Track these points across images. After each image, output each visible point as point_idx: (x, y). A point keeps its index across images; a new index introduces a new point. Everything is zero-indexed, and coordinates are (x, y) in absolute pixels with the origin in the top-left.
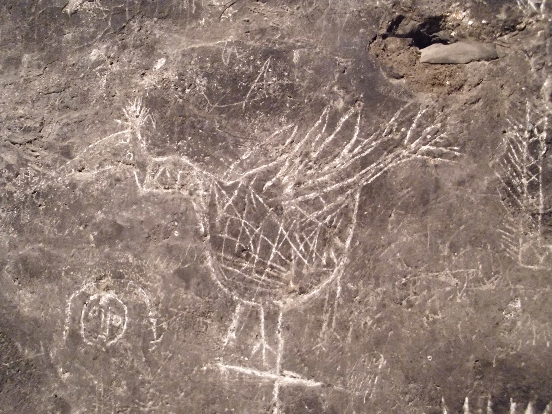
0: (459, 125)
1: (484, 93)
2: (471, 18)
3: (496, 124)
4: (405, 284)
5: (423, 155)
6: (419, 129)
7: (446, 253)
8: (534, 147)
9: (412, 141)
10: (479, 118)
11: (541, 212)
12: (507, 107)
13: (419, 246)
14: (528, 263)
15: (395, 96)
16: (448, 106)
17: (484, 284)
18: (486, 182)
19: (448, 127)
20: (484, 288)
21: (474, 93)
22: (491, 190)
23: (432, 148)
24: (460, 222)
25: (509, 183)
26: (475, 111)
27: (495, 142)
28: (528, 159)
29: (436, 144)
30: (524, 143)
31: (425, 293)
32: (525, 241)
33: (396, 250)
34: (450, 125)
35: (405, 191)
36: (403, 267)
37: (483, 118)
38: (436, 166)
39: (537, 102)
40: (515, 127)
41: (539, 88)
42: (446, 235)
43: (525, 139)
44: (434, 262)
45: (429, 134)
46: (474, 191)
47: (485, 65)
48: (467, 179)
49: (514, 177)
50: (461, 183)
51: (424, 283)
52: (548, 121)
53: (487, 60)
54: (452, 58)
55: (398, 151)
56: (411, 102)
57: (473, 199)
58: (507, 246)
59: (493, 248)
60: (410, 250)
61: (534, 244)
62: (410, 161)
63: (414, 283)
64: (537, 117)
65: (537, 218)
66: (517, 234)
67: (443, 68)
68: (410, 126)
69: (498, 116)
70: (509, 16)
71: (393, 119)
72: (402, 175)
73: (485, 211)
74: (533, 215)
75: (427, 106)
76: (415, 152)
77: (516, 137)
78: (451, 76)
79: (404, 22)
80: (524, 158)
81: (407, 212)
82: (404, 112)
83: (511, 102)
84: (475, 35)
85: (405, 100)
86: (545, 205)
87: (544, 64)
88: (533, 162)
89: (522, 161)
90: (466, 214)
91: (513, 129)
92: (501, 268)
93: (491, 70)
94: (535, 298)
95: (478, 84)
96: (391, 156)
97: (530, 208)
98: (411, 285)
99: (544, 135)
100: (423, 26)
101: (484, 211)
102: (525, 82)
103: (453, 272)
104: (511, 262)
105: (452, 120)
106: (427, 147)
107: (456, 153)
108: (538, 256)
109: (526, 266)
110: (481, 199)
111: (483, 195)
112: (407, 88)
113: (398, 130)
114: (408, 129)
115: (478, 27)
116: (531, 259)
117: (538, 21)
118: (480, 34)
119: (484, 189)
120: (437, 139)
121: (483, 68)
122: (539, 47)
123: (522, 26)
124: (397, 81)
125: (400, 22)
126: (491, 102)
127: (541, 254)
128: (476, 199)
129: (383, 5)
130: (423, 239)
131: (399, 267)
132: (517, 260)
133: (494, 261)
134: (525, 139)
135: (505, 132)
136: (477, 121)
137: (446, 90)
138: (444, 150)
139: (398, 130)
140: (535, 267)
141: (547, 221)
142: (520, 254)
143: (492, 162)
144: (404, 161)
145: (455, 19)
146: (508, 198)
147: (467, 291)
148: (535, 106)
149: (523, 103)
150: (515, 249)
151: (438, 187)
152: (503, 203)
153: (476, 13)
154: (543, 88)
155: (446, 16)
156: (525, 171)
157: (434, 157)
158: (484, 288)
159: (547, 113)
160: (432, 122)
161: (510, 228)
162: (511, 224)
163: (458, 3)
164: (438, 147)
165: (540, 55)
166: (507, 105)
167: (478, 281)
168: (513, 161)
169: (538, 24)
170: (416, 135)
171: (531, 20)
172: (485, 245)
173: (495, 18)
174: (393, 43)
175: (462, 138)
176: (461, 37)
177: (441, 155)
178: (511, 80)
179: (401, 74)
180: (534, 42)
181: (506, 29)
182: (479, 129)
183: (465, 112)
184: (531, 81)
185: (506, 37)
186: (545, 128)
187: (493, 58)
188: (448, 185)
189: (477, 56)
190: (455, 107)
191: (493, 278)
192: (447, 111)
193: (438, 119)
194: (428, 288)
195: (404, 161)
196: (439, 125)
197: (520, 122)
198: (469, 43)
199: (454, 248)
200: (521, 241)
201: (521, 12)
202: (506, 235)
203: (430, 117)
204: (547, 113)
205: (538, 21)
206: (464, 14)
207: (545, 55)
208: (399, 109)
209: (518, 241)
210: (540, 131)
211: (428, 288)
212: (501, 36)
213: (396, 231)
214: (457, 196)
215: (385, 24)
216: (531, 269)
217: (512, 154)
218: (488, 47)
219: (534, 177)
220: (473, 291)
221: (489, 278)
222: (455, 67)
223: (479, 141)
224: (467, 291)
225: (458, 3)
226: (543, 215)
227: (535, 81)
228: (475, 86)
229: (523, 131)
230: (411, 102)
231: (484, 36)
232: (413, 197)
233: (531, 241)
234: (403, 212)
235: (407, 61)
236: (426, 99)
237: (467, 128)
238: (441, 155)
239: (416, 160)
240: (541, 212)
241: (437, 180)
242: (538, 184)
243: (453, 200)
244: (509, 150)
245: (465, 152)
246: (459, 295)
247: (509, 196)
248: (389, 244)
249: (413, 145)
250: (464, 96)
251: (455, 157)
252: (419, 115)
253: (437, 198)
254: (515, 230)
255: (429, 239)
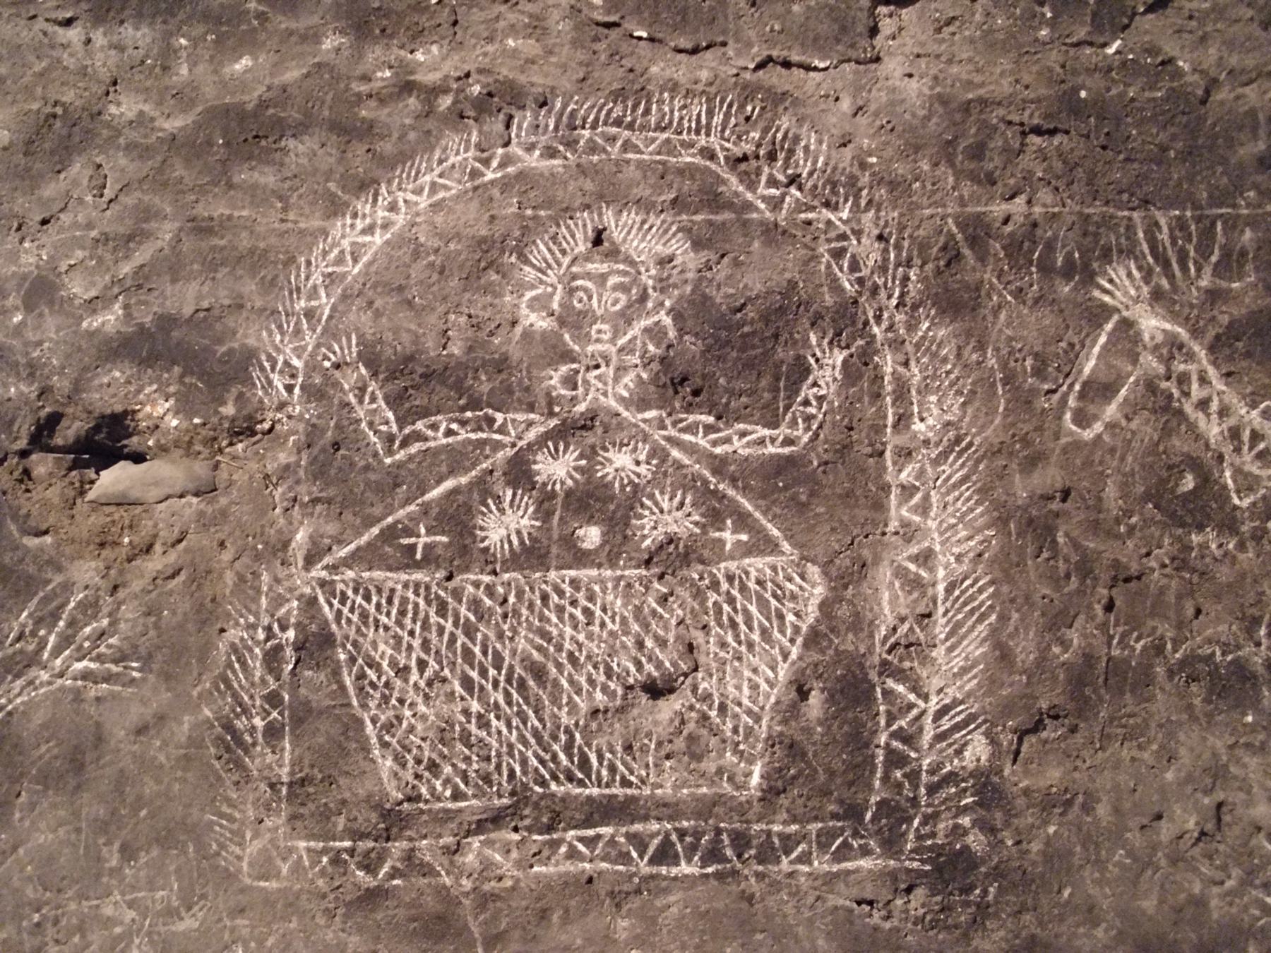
0: (141, 621)
1: (188, 558)
2: (177, 413)
3: (208, 616)
4: (38, 925)
5: (75, 679)
6: (70, 632)
7: (114, 863)
8: (273, 658)
9: (57, 652)
10: (178, 607)
11: (285, 779)
12: (230, 583)
13: (66, 851)
14: (260, 878)
15: (32, 569)
16: (124, 585)
17: (182, 919)
18: (186, 726)
19: (122, 625)
20: (181, 927)
21: (172, 557)
22: (195, 742)
23: (92, 665)
24: (139, 802)
25: (229, 727)
26: (171, 593)
27: (205, 652)
28: (263, 681)
29: (99, 658)
30: (257, 650)
31: (76, 939)
32: (256, 835)
33: (27, 860)
34: (127, 621)
35: (43, 748)
36: (36, 890)
37: (185, 606)
38: (98, 699)
39: (282, 572)
40: (242, 621)
41: (286, 545)
42: (113, 828)
43: (258, 643)
44: (92, 878)
45: (87, 639)
46: (165, 743)
47: (190, 505)
48: (152, 722)
49: (238, 716)
50: (141, 730)
51: (74, 921)
52: (299, 608)
53: (197, 495)
54: (135, 494)
55: (33, 672)
56: (58, 579)
57: (162, 758)
58: (222, 846)
59: (197, 851)
60: (51, 859)
61: (271, 841)
62: (52, 692)
63: (56, 922)
64: (279, 601)
65: (280, 791)
66: (243, 823)
67: (118, 514)
68: (55, 625)
69: (213, 600)
70: (238, 411)
71: (25, 614)
72: (38, 718)
73: (185, 780)
74: (272, 786)
75: (87, 587)
76: (61, 675)
77: (242, 639)
78: (131, 527)
79: (64, 423)
80: (256, 679)
81: (47, 788)
82: (46, 600)
83: (237, 573)
84: (185, 445)
85: (49, 575)
86: (293, 765)
87: (295, 500)
88: (273, 685)
89: (253, 684)
90: (150, 788)
91: (237, 624)
92: (209, 889)
93: (201, 514)
94: (269, 943)
95: (180, 541)
96: (19, 683)
97: (266, 773)
98: (49, 925)
99: (291, 634)
100: (97, 429)
101: (184, 780)
102: (262, 534)
103: (128, 897)
104: (230, 876)
105: (128, 612)
106: (85, 663)
107: (135, 674)
108: (279, 862)
109: (255, 884)
110: (178, 760)
111: (183, 751)
112: (53, 553)
113: (34, 634)
114: (49, 633)
115: (188, 431)
116: (265, 869)
117: (290, 417)
118: (190, 443)
119: (183, 739)
120: (102, 649)
121: (188, 511)
122: (287, 467)
123: (266, 426)
124: (37, 541)
125: (58, 423)
126: (200, 575)
127: (284, 859)
128: (168, 758)
129: (22, 394)
130: (73, 837)
131: (30, 892)
132: (240, 870)
133: (199, 876)
134: (258, 643)
135: (223, 630)
136: (174, 613)
137: (123, 552)
138: (114, 668)
139: (34, 634)
140: (273, 885)
141: (297, 796)
142: (246, 860)
143: (199, 688)
144: (42, 691)
145: (150, 416)
146: (226, 756)
147: (149, 934)
148: (277, 581)
149: (256, 575)
150: (237, 850)
151: (100, 739)
152: (217, 765)
153: (184, 407)
154: (293, 545)
155: (134, 412)
156: (258, 703)
157: (96, 683)
158: (181, 927)
159: (297, 593)
160: (95, 617)
161: (229, 811)
162: (232, 805)
163: (155, 387)
164: (103, 663)
165: (290, 482)
166: (230, 577)
167: (171, 913)
168: (236, 685)
169: (292, 423)
170: (66, 641)
171: (279, 416)
172: (185, 844)
173: (217, 412)
174: (42, 464)
175: (144, 645)
176: (163, 449)
177: (108, 678)
178: (238, 533)
179: (44, 528)
180: (283, 457)
181: (238, 434)
182: (181, 626)
183: (154, 595)
184: (272, 532)
185: (240, 446)
186: (293, 620)
187: (206, 490)
188: (119, 734)
189: (178, 489)
190: (136, 586)
191: (196, 908)
192: (121, 594)
193: (105, 610)
194: (81, 929)
195: (42, 691)
196: (105, 622)
197: (250, 611)
198: (173, 462)
199: (128, 852)
200: (248, 836)
201: (261, 401)
202: (221, 826)
203: (90, 608)
204: (297, 593)
205: (290, 417)
206: (167, 405)
207: (298, 482)
208: (36, 593)
209: (243, 837)
210: (284, 628)
211: (81, 929)
212: (231, 444)
213: (27, 823)
214: (134, 755)
215: (25, 428)
216: (264, 889)
217: (234, 672)
218: (201, 468)
219: (275, 714)
220: (159, 934)
221: (189, 909)
222: (139, 509)
223: (173, 652)
224: (149, 934)
225: (155, 387)
226: (291, 784)
227: (280, 532)
228: (173, 545)
229: (252, 627)
230: (58, 579)
231: (198, 447)
232: (56, 757)
233: (268, 836)
234: (39, 787)
235: (56, 500)
236: (86, 572)
237: (156, 626)
238: (108, 678)
239: (62, 689)
240: (285, 779)
241: (98, 725)
242: (283, 725)
243: (127, 763)
244: (230, 665)
245: (151, 671)
246: (137, 941)
247: (228, 749)
248: (15, 849)
249: (58, 662)
250: (155, 563)
251: (133, 680)
252: (72, 604)
253: (98, 759)
254: (237, 815)
255: (83, 837)
